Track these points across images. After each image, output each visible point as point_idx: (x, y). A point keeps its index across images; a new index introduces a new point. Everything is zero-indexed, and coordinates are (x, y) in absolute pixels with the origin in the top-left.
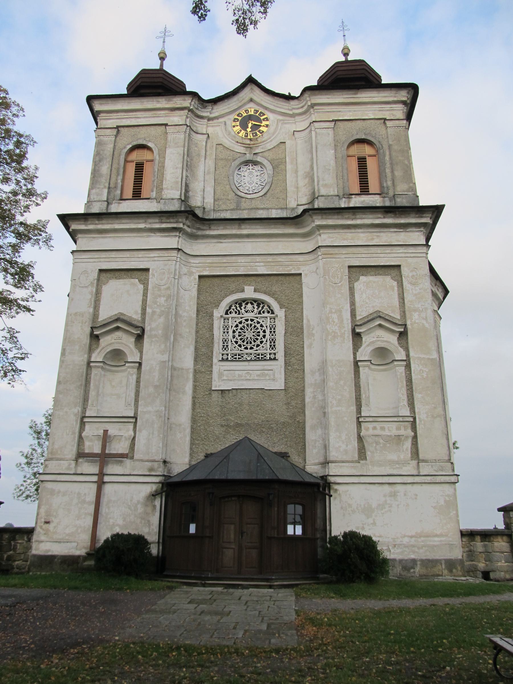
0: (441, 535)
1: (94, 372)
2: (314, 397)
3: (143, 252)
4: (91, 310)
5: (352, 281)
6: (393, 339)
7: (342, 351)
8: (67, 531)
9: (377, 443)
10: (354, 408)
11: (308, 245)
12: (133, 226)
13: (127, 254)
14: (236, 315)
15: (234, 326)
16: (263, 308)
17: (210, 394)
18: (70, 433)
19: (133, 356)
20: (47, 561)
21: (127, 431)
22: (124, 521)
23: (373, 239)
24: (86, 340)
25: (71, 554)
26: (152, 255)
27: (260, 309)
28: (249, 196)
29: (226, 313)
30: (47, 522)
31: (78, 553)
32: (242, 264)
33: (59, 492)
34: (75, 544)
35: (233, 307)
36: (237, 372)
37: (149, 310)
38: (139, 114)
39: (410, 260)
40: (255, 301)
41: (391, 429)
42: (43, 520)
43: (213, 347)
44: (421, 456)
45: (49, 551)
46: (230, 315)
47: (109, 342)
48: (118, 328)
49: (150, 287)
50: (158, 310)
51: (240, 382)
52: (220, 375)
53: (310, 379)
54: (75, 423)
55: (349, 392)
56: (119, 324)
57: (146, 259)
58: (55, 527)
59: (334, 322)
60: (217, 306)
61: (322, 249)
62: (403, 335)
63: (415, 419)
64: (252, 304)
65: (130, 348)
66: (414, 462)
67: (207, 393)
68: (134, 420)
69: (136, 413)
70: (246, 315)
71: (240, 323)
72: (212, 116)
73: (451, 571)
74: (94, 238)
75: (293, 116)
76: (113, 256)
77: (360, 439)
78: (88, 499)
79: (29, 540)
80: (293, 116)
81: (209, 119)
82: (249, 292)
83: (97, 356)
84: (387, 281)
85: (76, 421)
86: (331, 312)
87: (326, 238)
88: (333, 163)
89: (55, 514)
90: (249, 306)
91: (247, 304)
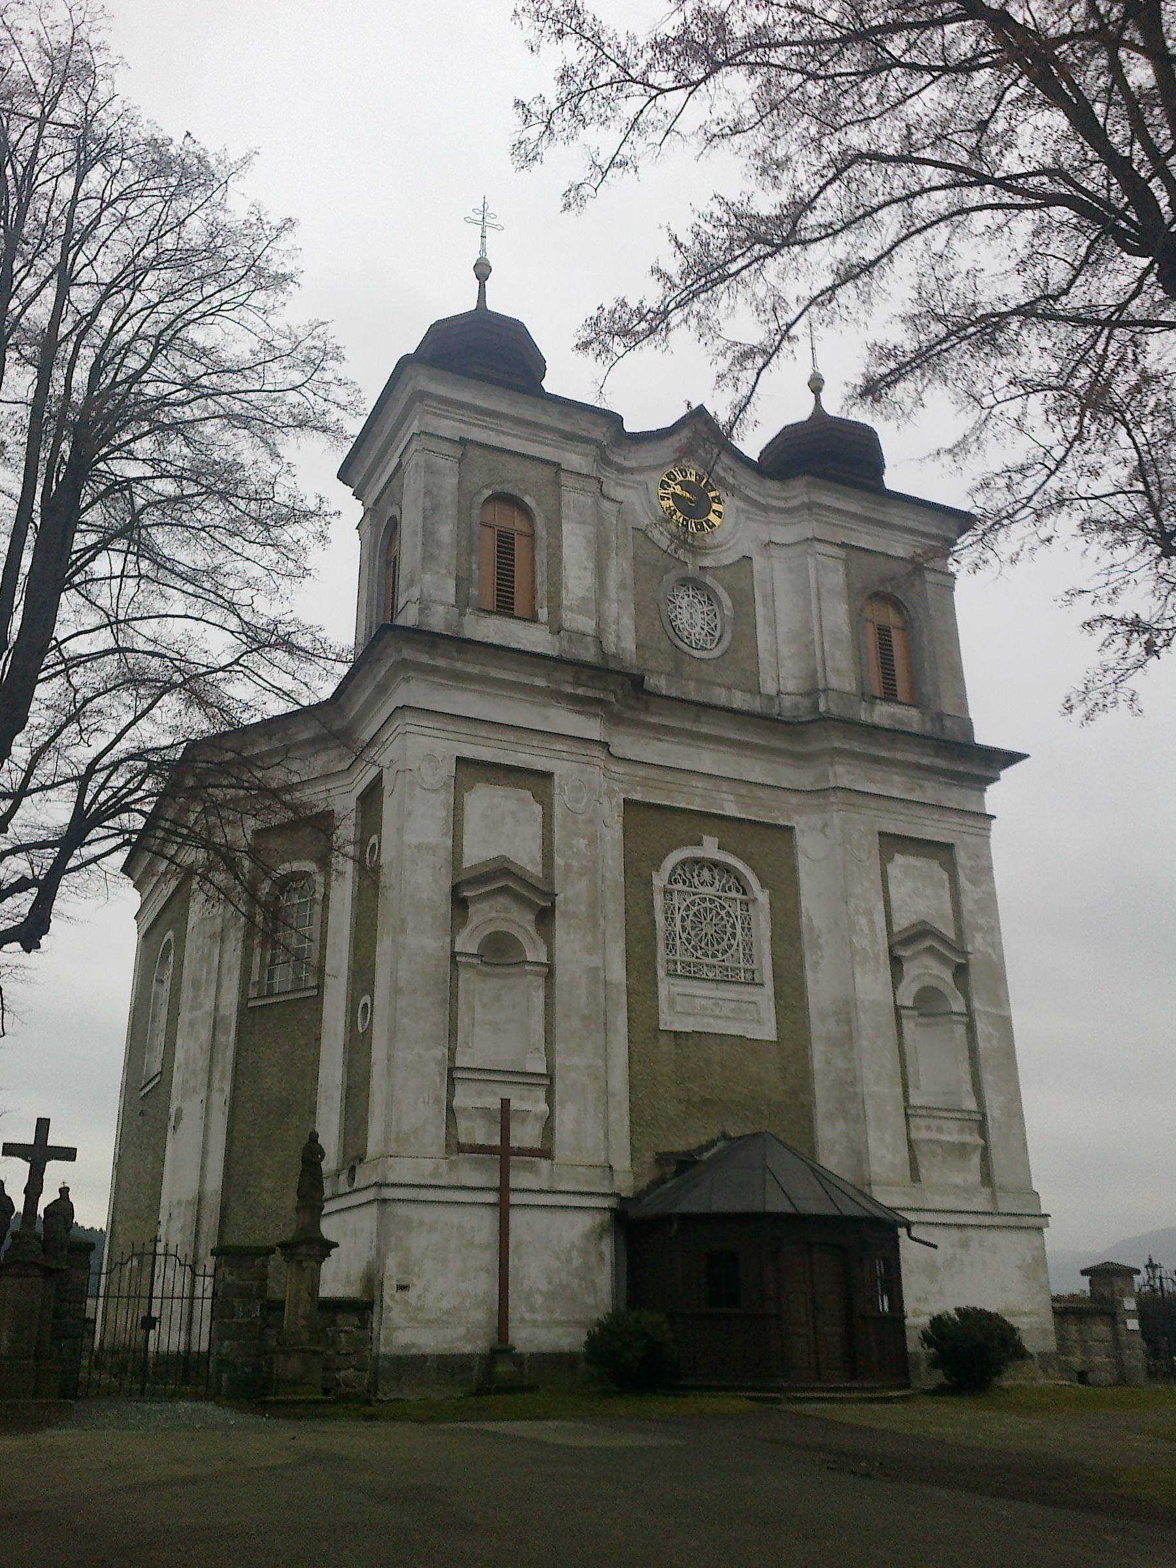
0: (1030, 1314)
1: (463, 975)
2: (828, 1062)
3: (540, 737)
4: (450, 843)
5: (885, 858)
6: (947, 975)
7: (872, 986)
8: (445, 1305)
9: (934, 1155)
10: (899, 1090)
11: (804, 778)
12: (525, 680)
13: (511, 736)
14: (685, 888)
15: (682, 908)
16: (728, 881)
17: (655, 1037)
18: (431, 1101)
19: (536, 953)
20: (411, 1365)
21: (530, 1103)
22: (550, 1282)
23: (912, 790)
24: (445, 906)
25: (456, 1351)
26: (557, 747)
27: (724, 881)
28: (695, 653)
29: (670, 882)
30: (403, 1288)
31: (468, 1349)
32: (698, 791)
33: (421, 1223)
34: (462, 1331)
35: (679, 871)
36: (698, 1001)
37: (559, 861)
38: (506, 426)
39: (967, 838)
40: (716, 866)
41: (951, 1134)
42: (394, 1283)
43: (656, 945)
44: (997, 1180)
45: (413, 1345)
46: (675, 887)
47: (489, 916)
48: (504, 890)
49: (558, 811)
50: (575, 863)
51: (706, 1020)
52: (672, 1002)
53: (821, 1028)
54: (438, 1079)
55: (889, 1058)
56: (500, 877)
57: (547, 753)
58: (419, 1297)
59: (862, 930)
60: (657, 866)
61: (840, 794)
62: (961, 972)
63: (984, 1115)
64: (710, 870)
65: (527, 931)
66: (986, 1191)
67: (650, 1035)
68: (546, 1082)
69: (550, 1066)
70: (701, 889)
71: (693, 903)
72: (627, 464)
73: (1045, 1371)
74: (442, 685)
75: (765, 508)
76: (483, 734)
77: (911, 1144)
78: (478, 1239)
79: (365, 1324)
80: (765, 508)
81: (621, 470)
82: (709, 848)
83: (467, 942)
84: (933, 868)
85: (441, 1074)
86: (857, 913)
87: (843, 775)
88: (846, 628)
89: (416, 1269)
90: (706, 874)
91: (701, 869)
